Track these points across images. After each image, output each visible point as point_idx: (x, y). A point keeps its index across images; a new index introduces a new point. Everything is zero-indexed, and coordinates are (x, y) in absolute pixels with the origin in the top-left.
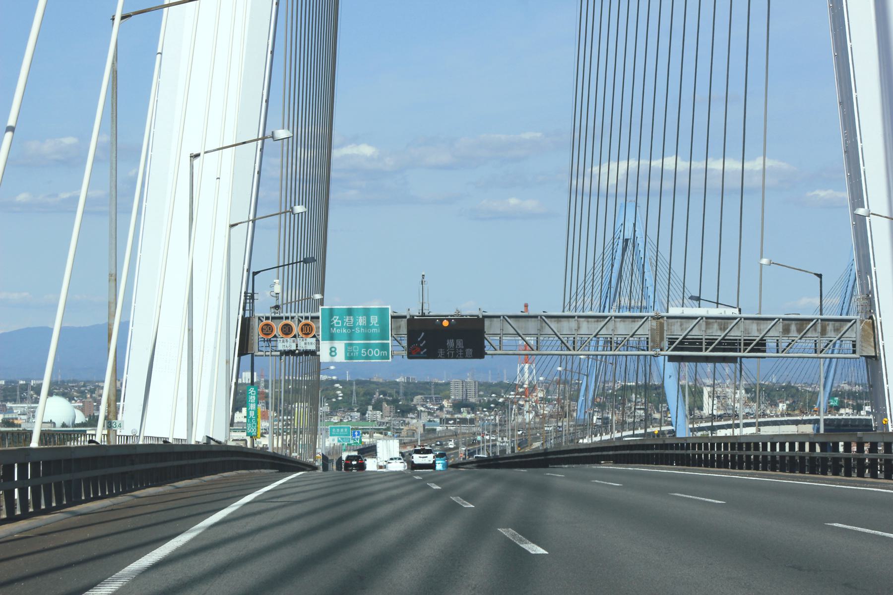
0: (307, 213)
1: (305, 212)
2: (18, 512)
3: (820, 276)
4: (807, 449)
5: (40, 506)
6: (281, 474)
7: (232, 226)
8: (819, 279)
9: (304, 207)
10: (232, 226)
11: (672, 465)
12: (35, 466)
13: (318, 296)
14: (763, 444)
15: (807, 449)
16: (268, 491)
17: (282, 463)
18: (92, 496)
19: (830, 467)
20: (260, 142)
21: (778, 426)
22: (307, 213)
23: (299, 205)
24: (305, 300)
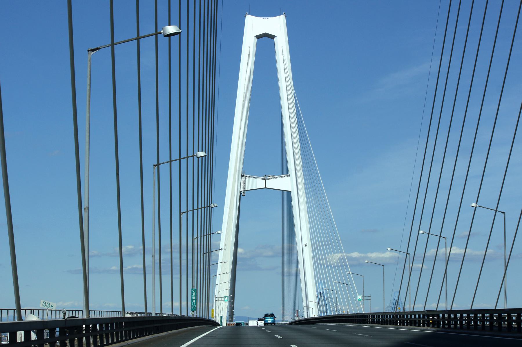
0: (207, 157)
1: (205, 156)
2: (115, 341)
3: (504, 213)
4: (409, 317)
5: (119, 339)
6: (214, 327)
7: (213, 276)
8: (504, 215)
9: (205, 152)
10: (213, 276)
11: (361, 323)
12: (121, 324)
13: (233, 306)
14: (368, 317)
15: (409, 317)
16: (213, 331)
17: (186, 322)
18: (135, 337)
19: (458, 325)
20: (212, 233)
21: (371, 312)
22: (207, 157)
23: (202, 151)
24: (204, 208)
